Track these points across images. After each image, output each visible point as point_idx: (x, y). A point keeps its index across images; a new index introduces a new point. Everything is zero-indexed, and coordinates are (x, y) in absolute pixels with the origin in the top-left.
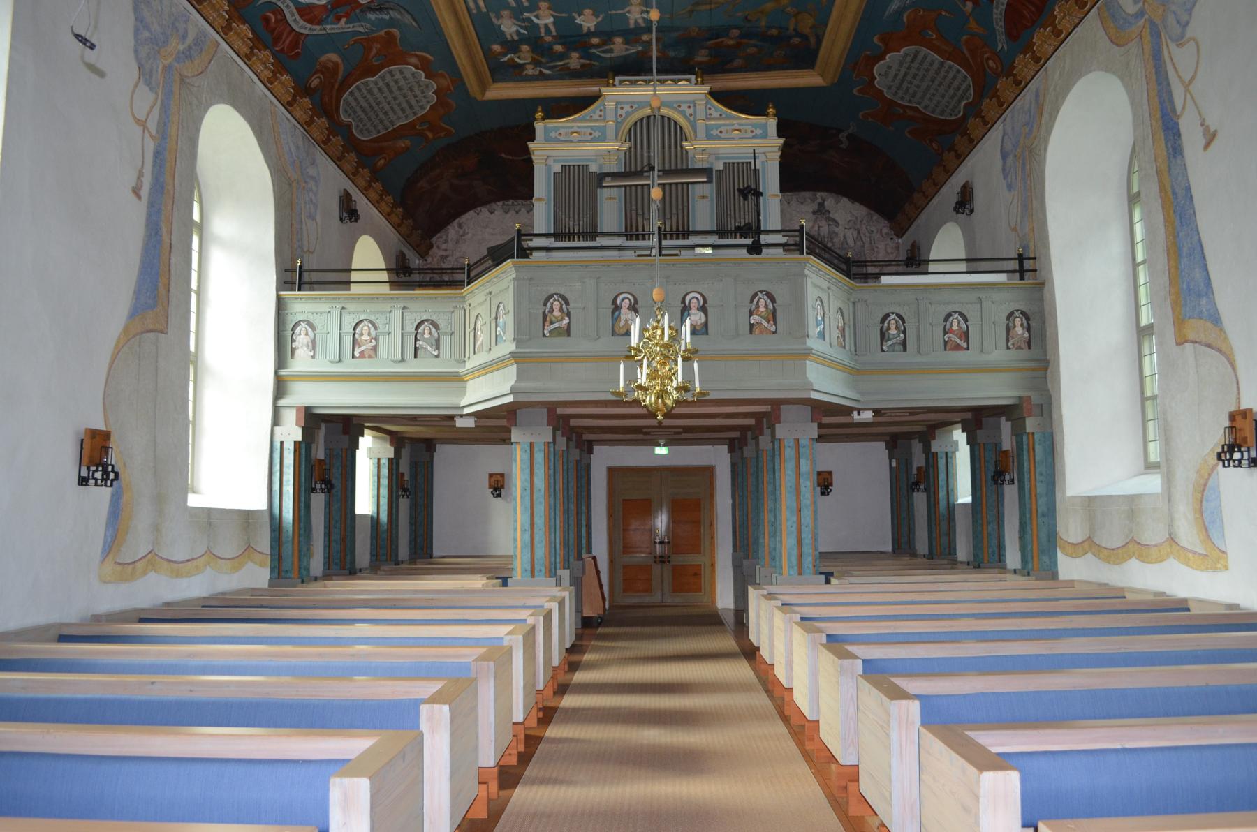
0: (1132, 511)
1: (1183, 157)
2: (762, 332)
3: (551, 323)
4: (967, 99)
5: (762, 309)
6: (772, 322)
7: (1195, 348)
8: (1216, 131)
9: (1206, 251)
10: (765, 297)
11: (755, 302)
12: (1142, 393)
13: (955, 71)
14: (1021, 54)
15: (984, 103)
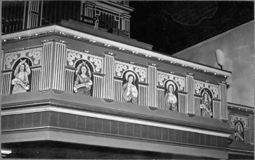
3: (80, 83)
5: (206, 100)
6: (210, 110)
10: (208, 93)
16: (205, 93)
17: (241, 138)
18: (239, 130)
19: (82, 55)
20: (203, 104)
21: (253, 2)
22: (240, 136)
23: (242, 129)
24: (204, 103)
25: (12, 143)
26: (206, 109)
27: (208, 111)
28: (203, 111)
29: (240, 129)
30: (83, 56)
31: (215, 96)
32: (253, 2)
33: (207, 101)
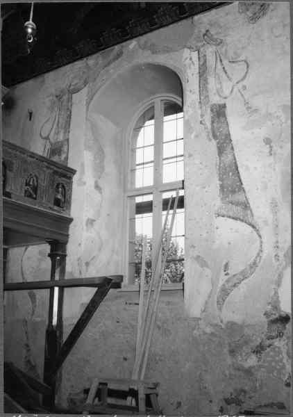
1: (226, 118)
23: (36, 184)
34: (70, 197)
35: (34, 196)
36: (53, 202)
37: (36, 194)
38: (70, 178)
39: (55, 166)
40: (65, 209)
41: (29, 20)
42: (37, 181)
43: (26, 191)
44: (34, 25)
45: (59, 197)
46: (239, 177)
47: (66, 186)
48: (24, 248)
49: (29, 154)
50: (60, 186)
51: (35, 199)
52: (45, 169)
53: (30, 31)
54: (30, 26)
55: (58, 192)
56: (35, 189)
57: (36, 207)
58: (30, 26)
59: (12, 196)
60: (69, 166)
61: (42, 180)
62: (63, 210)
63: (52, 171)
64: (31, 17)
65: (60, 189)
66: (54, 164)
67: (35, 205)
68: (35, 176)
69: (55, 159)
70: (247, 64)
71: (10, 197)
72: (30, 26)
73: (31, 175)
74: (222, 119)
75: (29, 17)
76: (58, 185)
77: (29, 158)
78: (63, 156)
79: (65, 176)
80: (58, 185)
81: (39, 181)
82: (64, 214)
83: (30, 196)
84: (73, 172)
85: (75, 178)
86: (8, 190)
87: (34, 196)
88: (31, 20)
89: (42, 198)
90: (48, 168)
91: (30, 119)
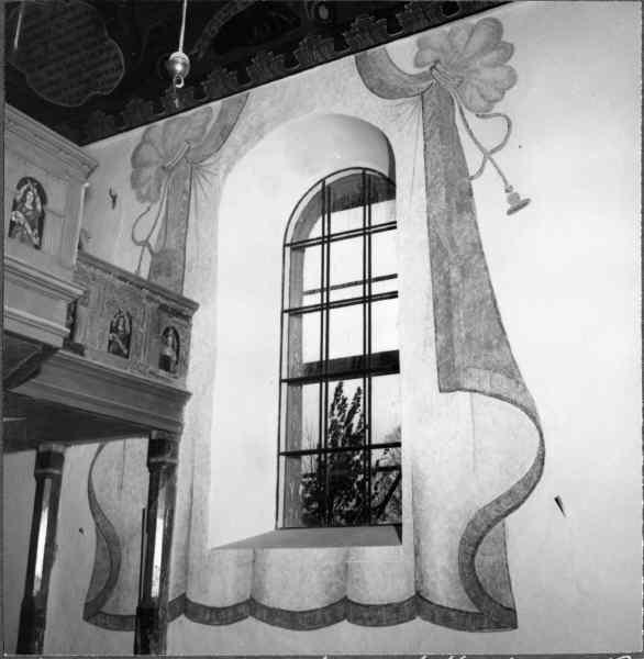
0: (347, 566)
1: (473, 214)
2: (22, 240)
4: (102, 90)
5: (28, 205)
6: (36, 231)
7: (472, 397)
8: (528, 200)
9: (500, 304)
10: (35, 191)
11: (22, 191)
12: (279, 450)
13: (112, 54)
14: (223, 67)
15: (132, 102)
16: (29, 189)
17: (122, 346)
18: (120, 328)
19: (346, 597)
20: (21, 211)
21: (398, 372)
22: (120, 343)
23: (128, 329)
24: (24, 210)
25: (265, 535)
26: (23, 226)
27: (30, 231)
28: (15, 228)
29: (124, 326)
30: (349, 598)
31: (50, 205)
32: (398, 372)
33: (31, 208)
34: (187, 353)
35: (125, 352)
36: (157, 361)
37: (128, 347)
38: (188, 318)
39: (162, 296)
40: (177, 374)
41: (177, 50)
42: (131, 323)
43: (110, 343)
44: (187, 58)
45: (169, 352)
46: (499, 320)
47: (179, 332)
48: (96, 446)
49: (118, 274)
50: (171, 332)
51: (127, 357)
52: (144, 301)
53: (179, 68)
54: (180, 60)
55: (166, 344)
56: (127, 339)
57: (128, 372)
58: (180, 60)
59: (86, 352)
60: (186, 295)
61: (138, 322)
62: (176, 378)
63: (157, 305)
64: (181, 44)
65: (170, 339)
66: (162, 292)
67: (126, 369)
68: (128, 314)
69: (161, 281)
70: (508, 119)
71: (82, 354)
72: (180, 60)
73: (120, 312)
74: (467, 217)
75: (178, 43)
76: (167, 330)
77: (118, 282)
78: (175, 278)
79: (178, 314)
80: (167, 330)
81: (135, 324)
82: (176, 384)
83: (118, 352)
84: (193, 306)
85: (198, 318)
86: (78, 340)
87: (125, 352)
88: (181, 49)
89: (138, 355)
90: (149, 299)
91: (114, 207)
